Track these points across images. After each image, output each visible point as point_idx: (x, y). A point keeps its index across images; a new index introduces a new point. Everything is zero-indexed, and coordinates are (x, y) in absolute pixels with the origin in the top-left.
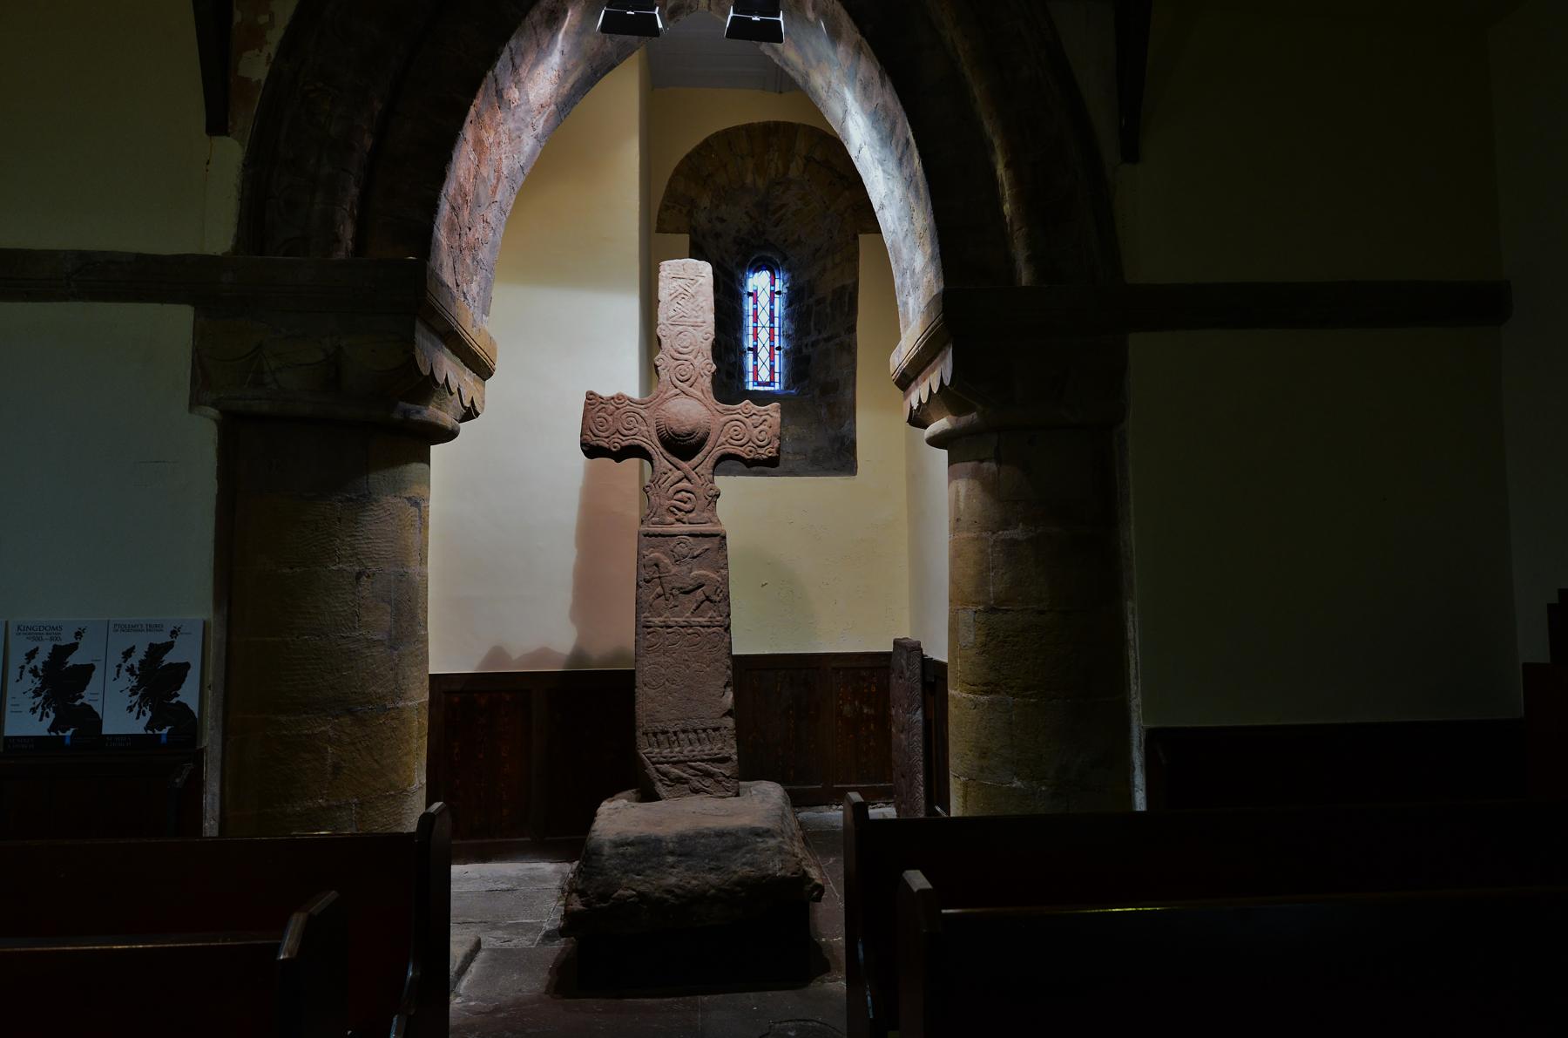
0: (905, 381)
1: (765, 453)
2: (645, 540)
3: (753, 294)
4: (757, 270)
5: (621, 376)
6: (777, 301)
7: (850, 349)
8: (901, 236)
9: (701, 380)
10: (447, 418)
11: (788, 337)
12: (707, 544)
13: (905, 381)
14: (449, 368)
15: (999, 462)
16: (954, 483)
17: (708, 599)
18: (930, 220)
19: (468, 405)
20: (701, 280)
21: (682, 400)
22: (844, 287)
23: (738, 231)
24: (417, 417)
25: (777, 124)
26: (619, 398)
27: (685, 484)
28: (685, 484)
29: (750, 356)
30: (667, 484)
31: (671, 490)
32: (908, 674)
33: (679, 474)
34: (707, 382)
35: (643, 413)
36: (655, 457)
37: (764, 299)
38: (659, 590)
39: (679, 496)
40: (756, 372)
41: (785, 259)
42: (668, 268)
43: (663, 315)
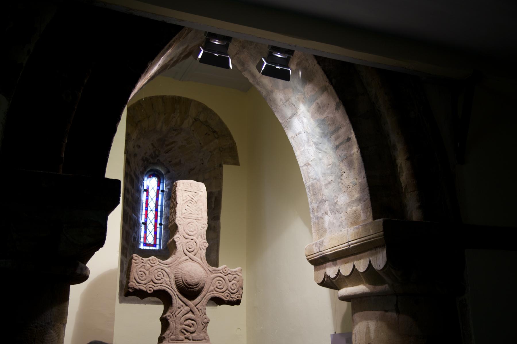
3: (147, 191)
4: (150, 176)
6: (160, 196)
9: (200, 251)
15: (398, 312)
18: (362, 179)
20: (200, 193)
23: (145, 154)
25: (180, 98)
27: (190, 315)
28: (190, 315)
29: (143, 227)
31: (183, 319)
33: (187, 308)
34: (203, 253)
35: (167, 270)
37: (153, 194)
39: (187, 322)
40: (145, 238)
41: (168, 172)
43: (180, 210)
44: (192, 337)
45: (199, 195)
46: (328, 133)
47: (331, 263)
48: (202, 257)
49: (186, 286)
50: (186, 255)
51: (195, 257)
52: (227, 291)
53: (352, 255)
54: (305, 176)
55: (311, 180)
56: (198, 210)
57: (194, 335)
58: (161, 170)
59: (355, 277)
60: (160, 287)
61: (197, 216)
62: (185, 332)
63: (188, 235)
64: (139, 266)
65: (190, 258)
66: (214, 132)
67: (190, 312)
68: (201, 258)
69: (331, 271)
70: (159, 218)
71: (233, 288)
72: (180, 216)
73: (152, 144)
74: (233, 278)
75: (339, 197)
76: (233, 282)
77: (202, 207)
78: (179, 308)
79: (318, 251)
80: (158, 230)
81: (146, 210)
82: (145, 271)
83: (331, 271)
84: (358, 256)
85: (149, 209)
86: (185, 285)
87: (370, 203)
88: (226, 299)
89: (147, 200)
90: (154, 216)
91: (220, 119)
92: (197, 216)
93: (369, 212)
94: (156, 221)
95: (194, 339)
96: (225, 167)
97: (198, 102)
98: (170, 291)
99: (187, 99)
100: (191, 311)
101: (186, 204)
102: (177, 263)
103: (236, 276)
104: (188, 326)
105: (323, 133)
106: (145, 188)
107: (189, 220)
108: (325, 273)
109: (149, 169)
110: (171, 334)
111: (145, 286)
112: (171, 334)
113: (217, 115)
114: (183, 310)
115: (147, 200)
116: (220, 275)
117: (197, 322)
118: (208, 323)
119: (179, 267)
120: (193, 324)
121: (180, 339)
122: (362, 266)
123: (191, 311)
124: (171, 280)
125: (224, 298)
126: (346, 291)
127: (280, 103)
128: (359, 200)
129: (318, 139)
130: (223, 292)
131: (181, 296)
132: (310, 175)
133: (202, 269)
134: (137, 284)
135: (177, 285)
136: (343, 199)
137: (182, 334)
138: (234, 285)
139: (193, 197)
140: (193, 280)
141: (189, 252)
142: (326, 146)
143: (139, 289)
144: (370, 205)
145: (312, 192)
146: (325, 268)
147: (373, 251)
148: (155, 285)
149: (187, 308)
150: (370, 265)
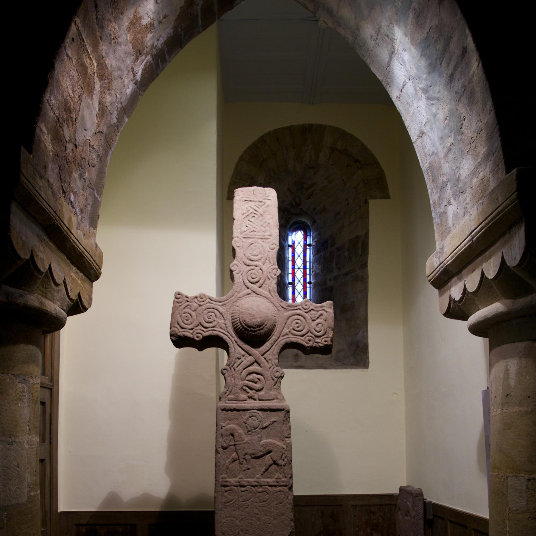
0: (442, 281)
1: (321, 342)
2: (223, 414)
3: (293, 246)
4: (295, 230)
5: (203, 281)
6: (308, 252)
7: (363, 280)
8: (442, 155)
9: (268, 282)
10: (54, 307)
11: (316, 275)
12: (274, 417)
13: (442, 281)
14: (49, 258)
16: (500, 366)
17: (275, 463)
18: (489, 117)
19: (74, 297)
20: (268, 202)
21: (253, 298)
22: (358, 237)
24: (21, 301)
25: (311, 126)
26: (201, 298)
27: (255, 367)
28: (255, 367)
30: (241, 368)
32: (413, 514)
33: (250, 359)
35: (221, 309)
36: (231, 345)
37: (299, 250)
38: (234, 455)
39: (250, 377)
41: (314, 222)
42: (240, 193)
43: (238, 229)
44: (258, 396)
45: (265, 205)
46: (436, 60)
47: (455, 278)
48: (271, 288)
49: (246, 329)
50: (248, 288)
51: (260, 289)
52: (309, 334)
53: (480, 255)
54: (420, 155)
55: (428, 157)
56: (265, 225)
57: (260, 393)
58: (306, 221)
59: (486, 290)
60: (211, 332)
61: (264, 234)
62: (248, 390)
63: (251, 260)
64: (183, 306)
65: (254, 292)
66: (357, 161)
67: (255, 364)
68: (270, 291)
69: (455, 292)
70: (308, 276)
71: (318, 329)
72: (239, 235)
73: (289, 189)
74: (317, 315)
75: (462, 166)
76: (318, 321)
77: (270, 221)
78: (239, 359)
79: (438, 263)
80: (308, 289)
81: (293, 269)
82: (190, 312)
83: (455, 292)
84: (487, 253)
85: (296, 267)
86: (244, 327)
87: (501, 153)
88: (307, 345)
89: (293, 256)
90: (302, 275)
91: (363, 145)
92: (264, 234)
93: (500, 171)
94: (305, 280)
95: (261, 398)
96: (371, 202)
97: (334, 127)
98: (225, 337)
99: (320, 126)
100: (256, 362)
101: (247, 219)
102: (235, 299)
103: (323, 312)
104: (252, 382)
105: (430, 64)
106: (290, 243)
107: (251, 240)
108: (450, 297)
109: (292, 222)
110: (228, 392)
111: (191, 331)
112: (228, 392)
113: (357, 140)
114: (245, 362)
115: (293, 256)
116: (298, 312)
117: (265, 376)
118: (282, 377)
119: (237, 304)
120: (259, 379)
121: (241, 399)
122: (491, 268)
123: (256, 362)
124: (226, 322)
125: (304, 343)
126: (475, 317)
127: (371, 43)
128: (487, 157)
129: (426, 80)
130: (302, 336)
131: (240, 343)
132: (426, 151)
133: (271, 305)
134: (181, 330)
135: (234, 329)
136: (467, 166)
137: (244, 392)
138: (320, 325)
139: (257, 209)
140: (254, 320)
141: (252, 283)
142: (437, 88)
143: (184, 335)
144: (502, 157)
145: (431, 178)
146: (450, 288)
147: (507, 236)
148: (205, 330)
149: (250, 359)
150: (503, 262)
